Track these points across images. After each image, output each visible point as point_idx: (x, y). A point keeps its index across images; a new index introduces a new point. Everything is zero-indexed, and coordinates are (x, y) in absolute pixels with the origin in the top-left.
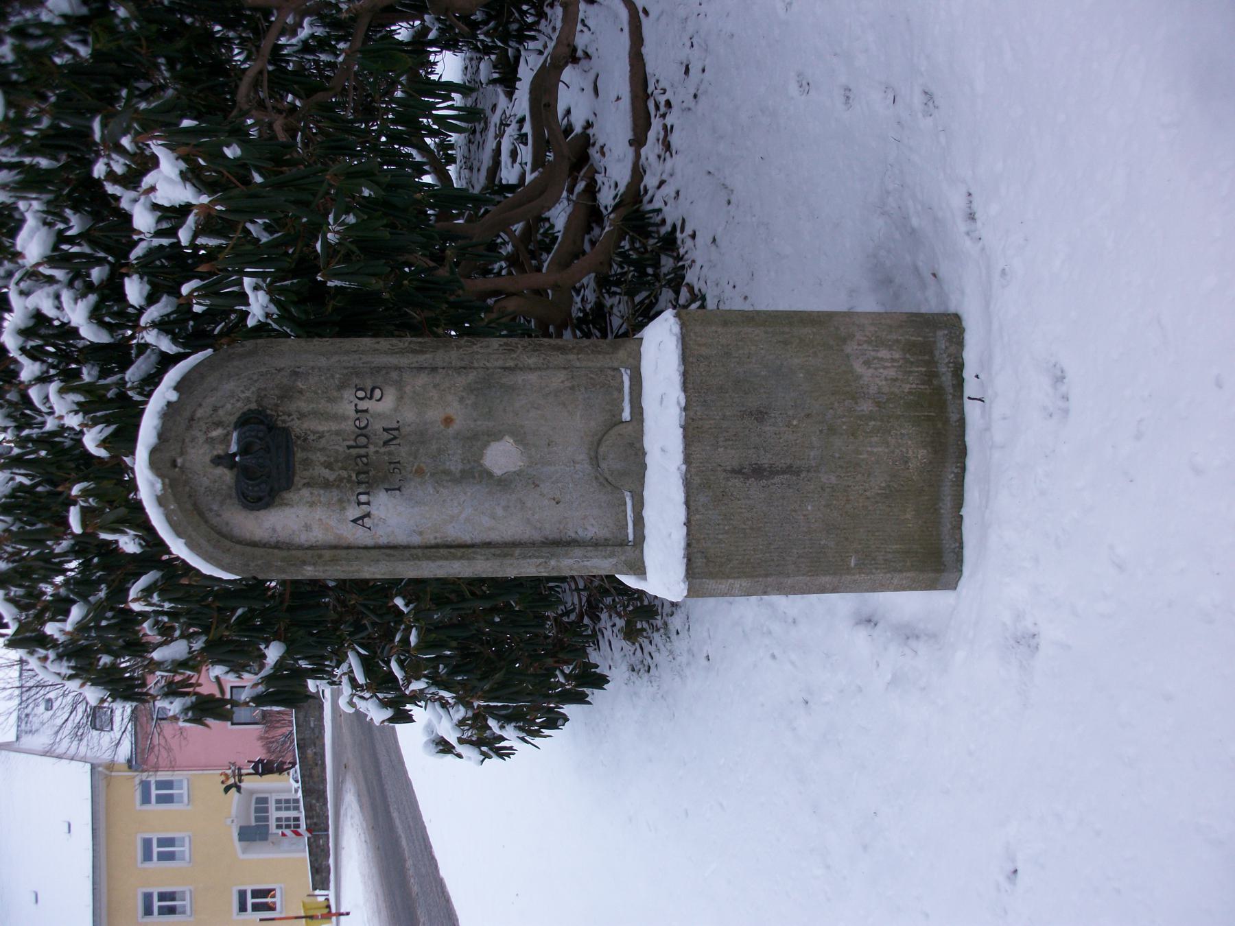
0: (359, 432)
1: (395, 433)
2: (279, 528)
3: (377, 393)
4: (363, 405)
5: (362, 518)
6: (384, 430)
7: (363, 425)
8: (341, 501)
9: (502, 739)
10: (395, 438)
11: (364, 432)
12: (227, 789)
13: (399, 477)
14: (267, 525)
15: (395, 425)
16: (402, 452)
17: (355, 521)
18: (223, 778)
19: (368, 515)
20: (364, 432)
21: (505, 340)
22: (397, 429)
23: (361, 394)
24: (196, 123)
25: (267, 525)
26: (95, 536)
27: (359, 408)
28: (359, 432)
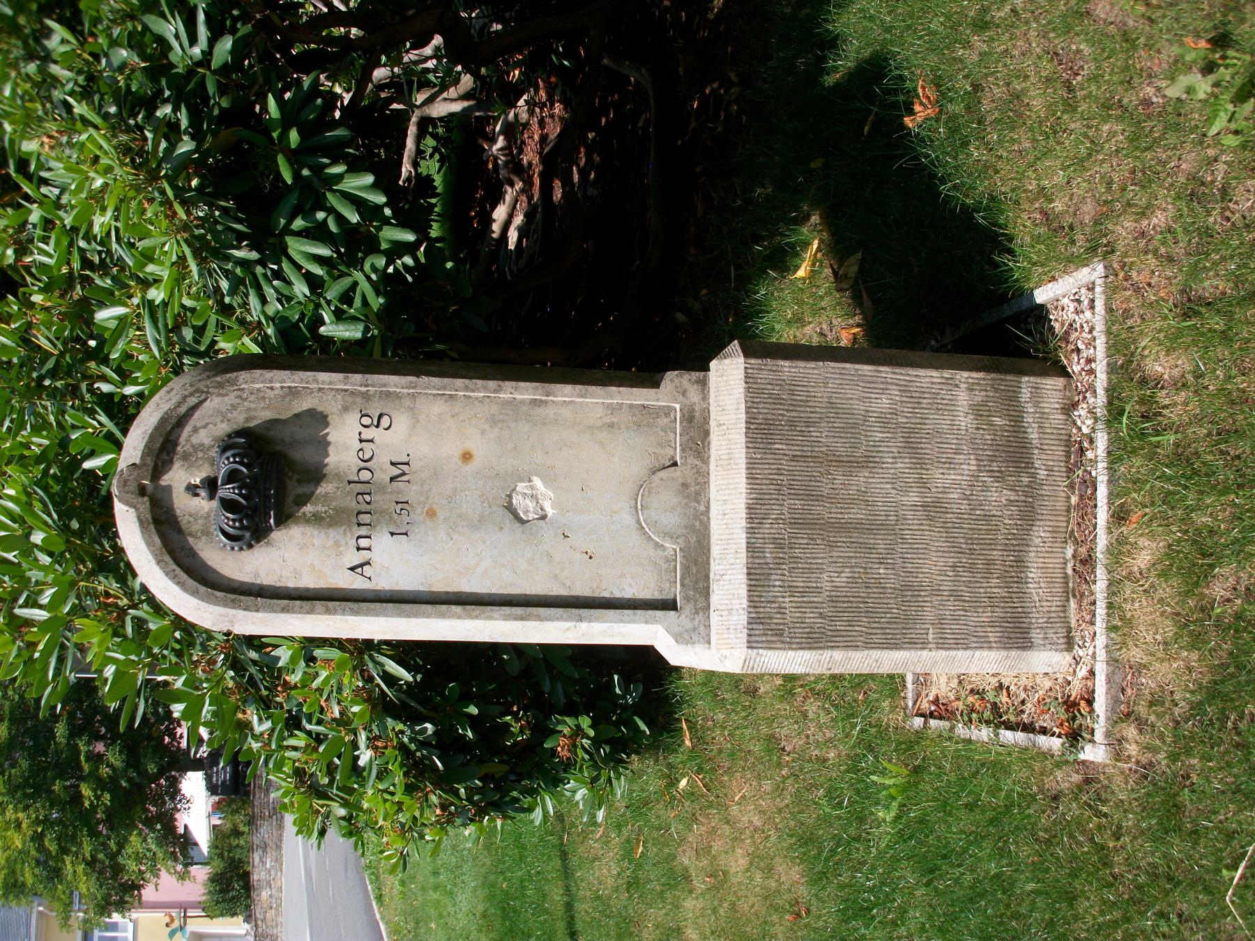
0: (363, 464)
1: (405, 468)
2: (262, 573)
3: (385, 421)
4: (367, 434)
5: (361, 565)
6: (392, 464)
7: (367, 457)
8: (337, 544)
9: (62, 296)
10: (404, 474)
11: (367, 465)
12: (172, 934)
13: (408, 519)
14: (249, 568)
15: (405, 460)
16: (411, 492)
17: (352, 569)
18: (167, 919)
19: (368, 563)
20: (367, 465)
21: (165, 389)
22: (407, 464)
23: (366, 421)
24: (119, 508)
25: (249, 568)
26: (277, 152)
27: (363, 437)
28: (363, 464)
